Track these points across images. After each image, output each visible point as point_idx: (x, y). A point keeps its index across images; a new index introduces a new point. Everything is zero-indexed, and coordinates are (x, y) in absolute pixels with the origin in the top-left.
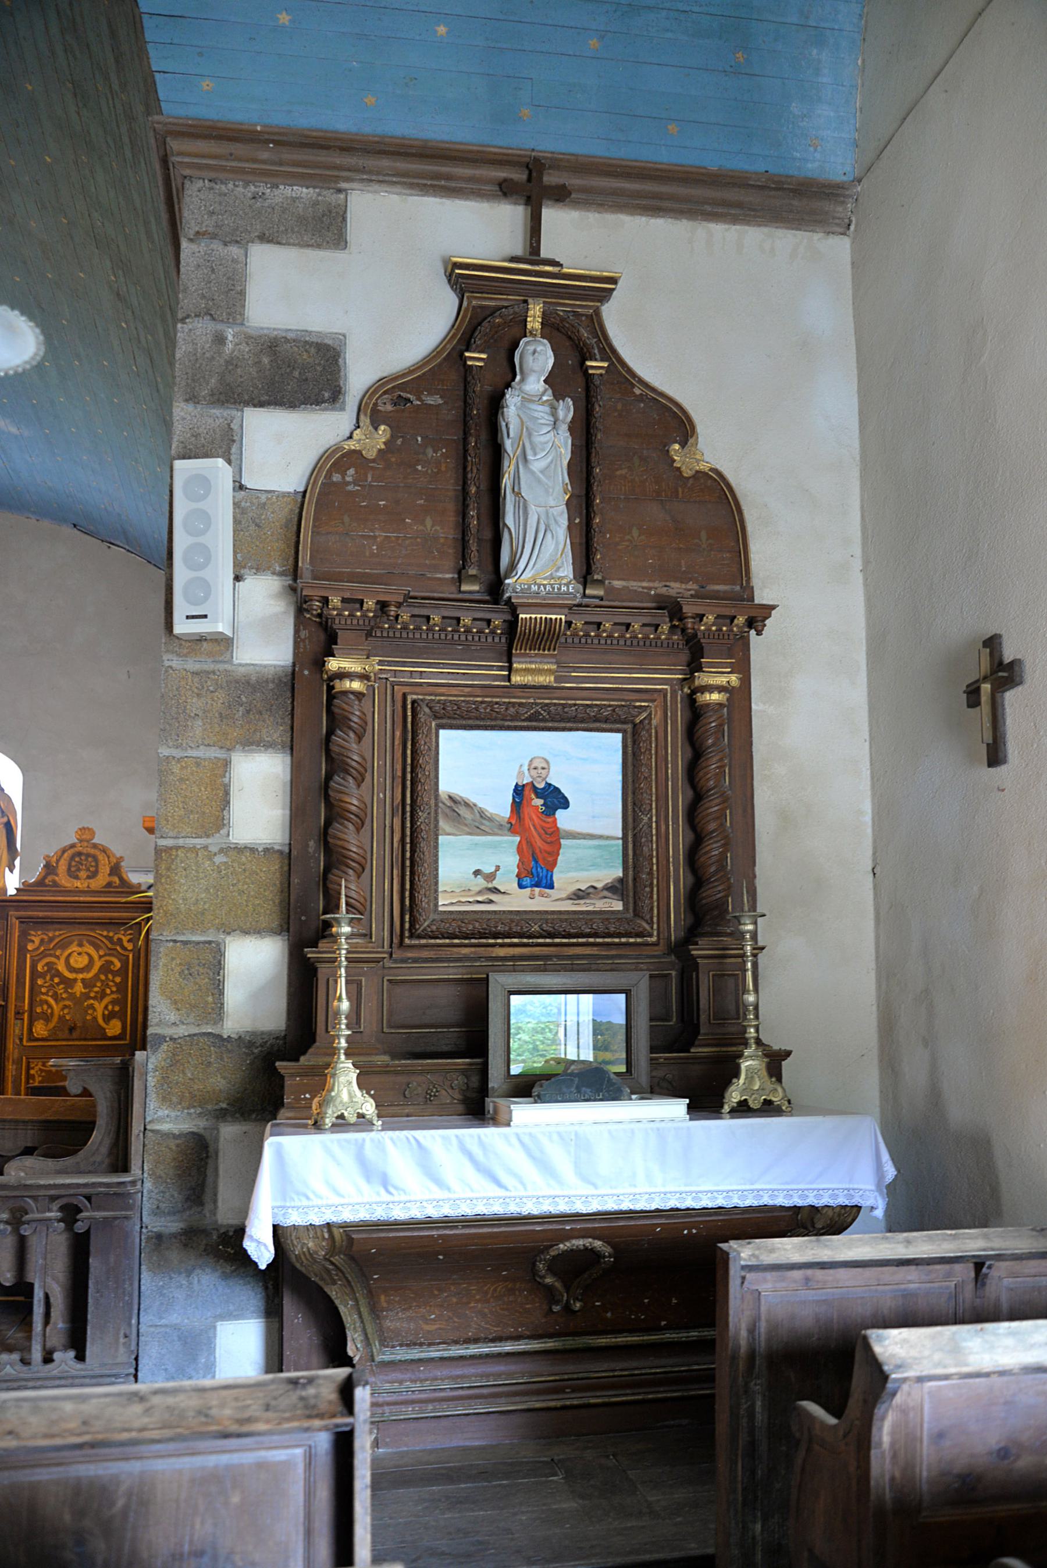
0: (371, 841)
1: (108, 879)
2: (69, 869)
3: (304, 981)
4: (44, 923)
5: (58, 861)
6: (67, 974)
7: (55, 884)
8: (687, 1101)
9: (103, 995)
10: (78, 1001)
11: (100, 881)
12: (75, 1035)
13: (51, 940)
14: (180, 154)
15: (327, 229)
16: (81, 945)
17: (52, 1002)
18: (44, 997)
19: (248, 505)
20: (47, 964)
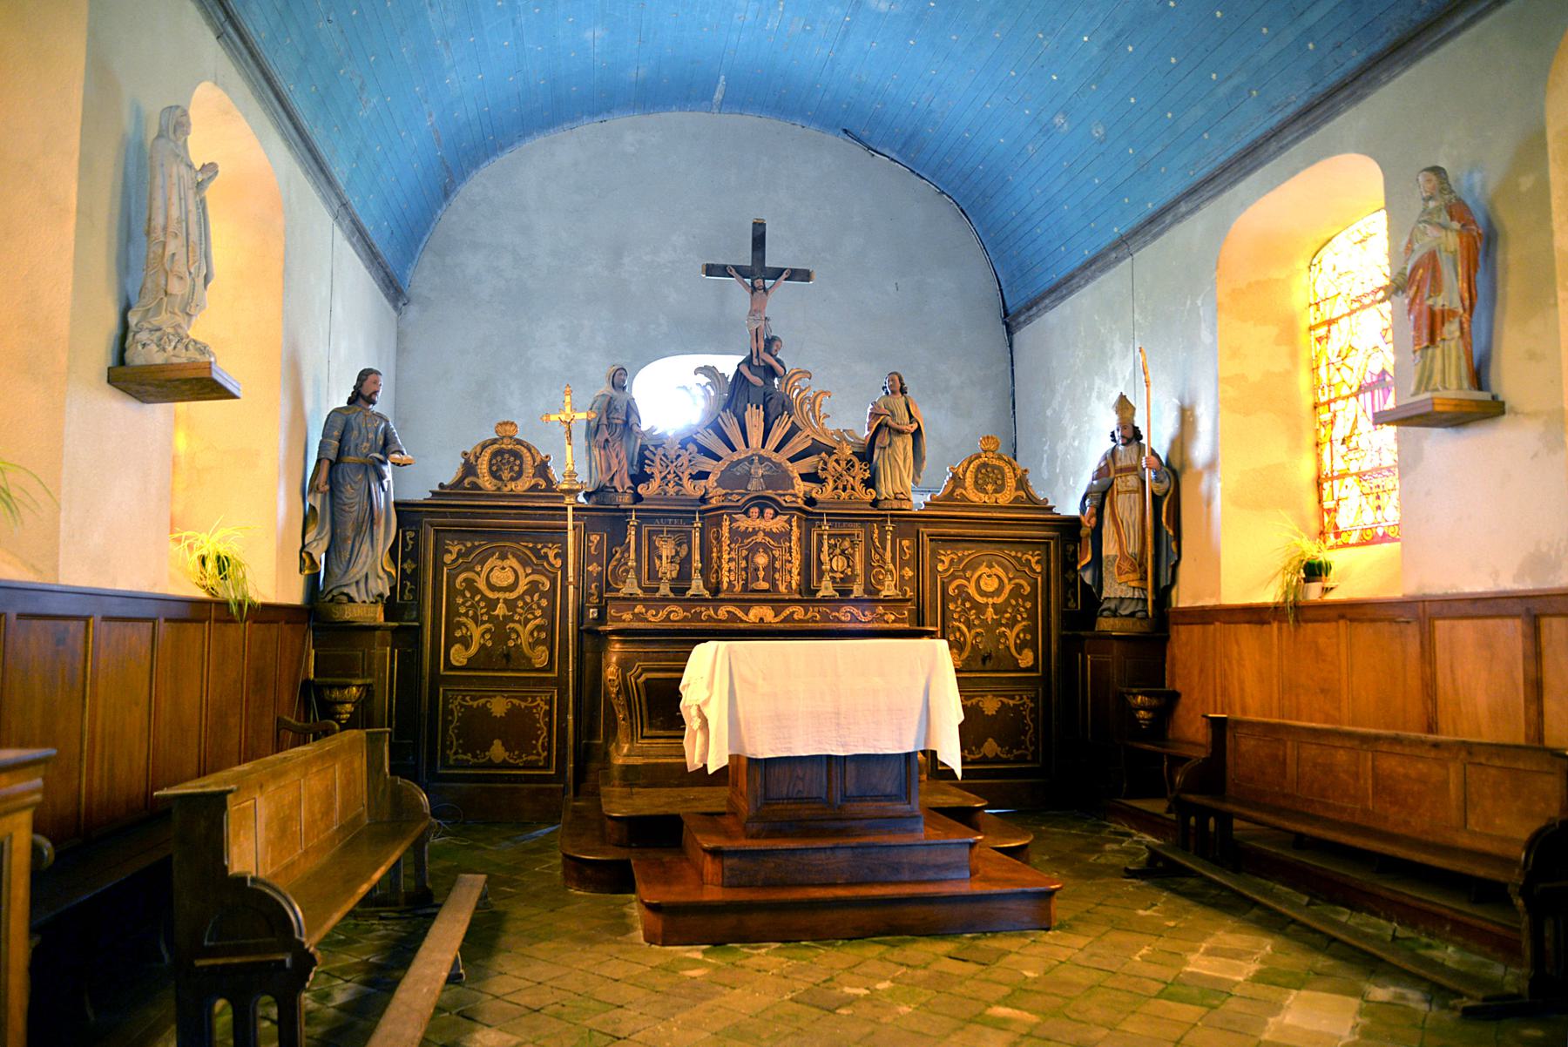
1: (1014, 494)
2: (976, 482)
4: (461, 534)
5: (965, 472)
6: (491, 595)
7: (964, 498)
9: (1012, 623)
10: (990, 628)
11: (1005, 498)
12: (989, 665)
13: (961, 560)
16: (990, 566)
17: (964, 628)
18: (463, 619)
20: (465, 580)
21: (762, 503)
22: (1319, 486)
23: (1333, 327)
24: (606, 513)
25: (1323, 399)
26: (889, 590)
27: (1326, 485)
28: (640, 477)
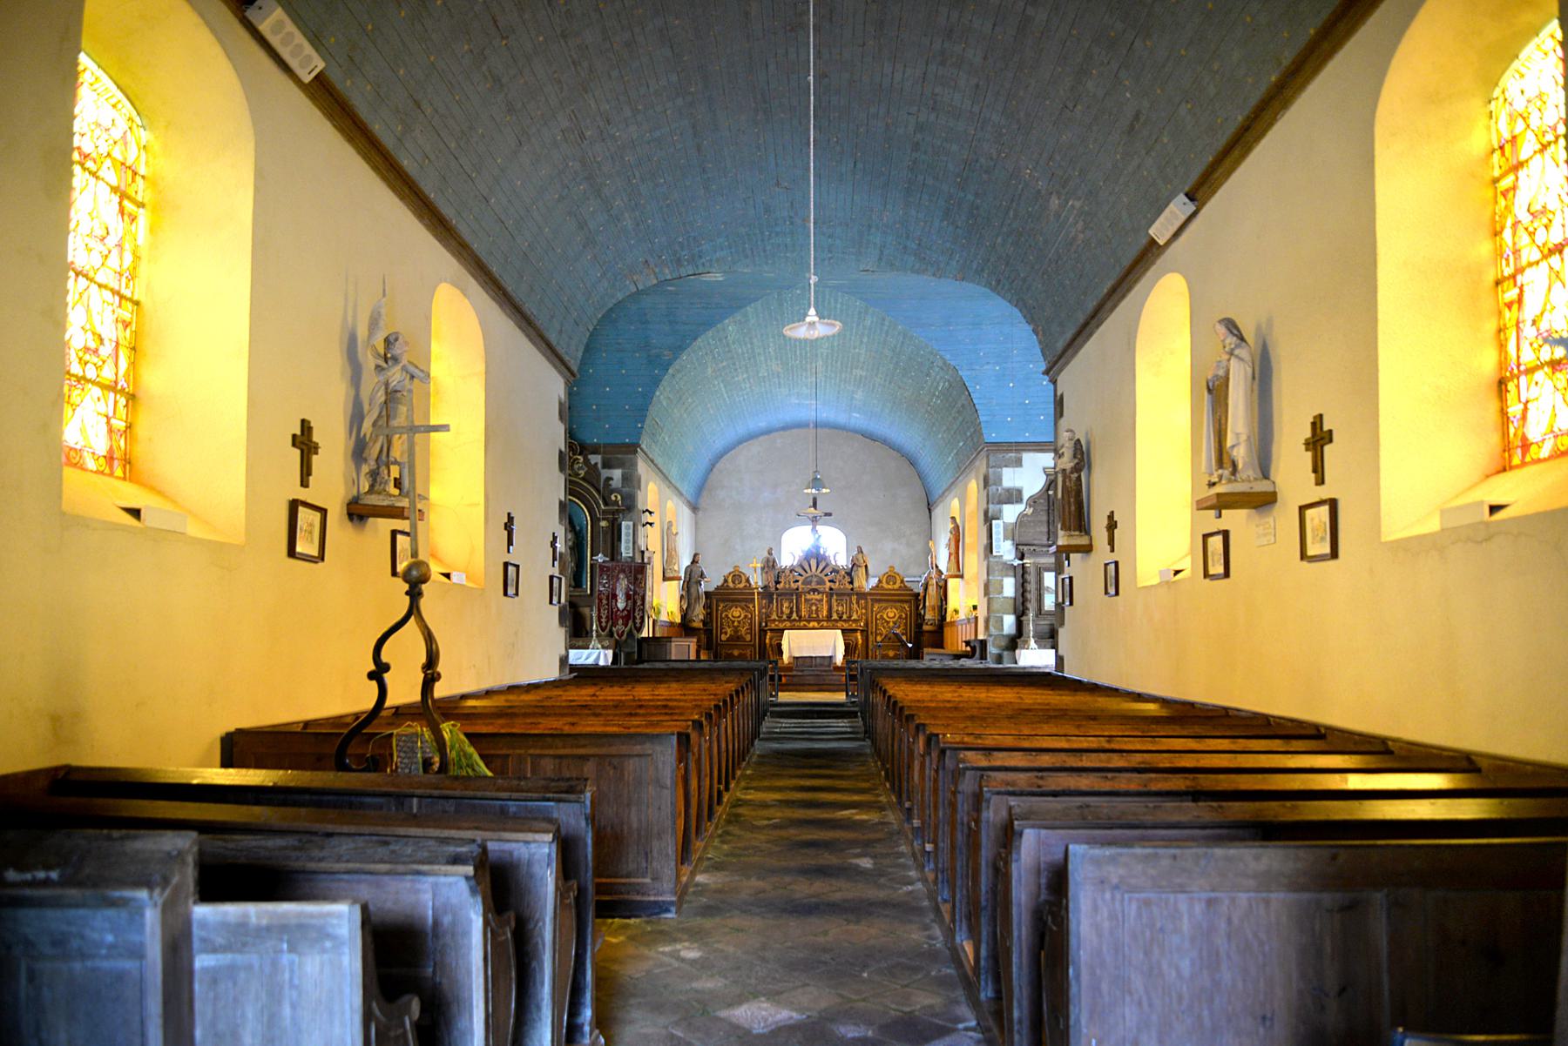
0: (1032, 596)
3: (1020, 625)
8: (839, 659)
14: (910, 964)
15: (1018, 463)
19: (1006, 525)
21: (814, 590)
22: (1502, 384)
23: (1521, 173)
24: (767, 593)
25: (1508, 271)
26: (855, 617)
27: (1511, 386)
28: (778, 582)
